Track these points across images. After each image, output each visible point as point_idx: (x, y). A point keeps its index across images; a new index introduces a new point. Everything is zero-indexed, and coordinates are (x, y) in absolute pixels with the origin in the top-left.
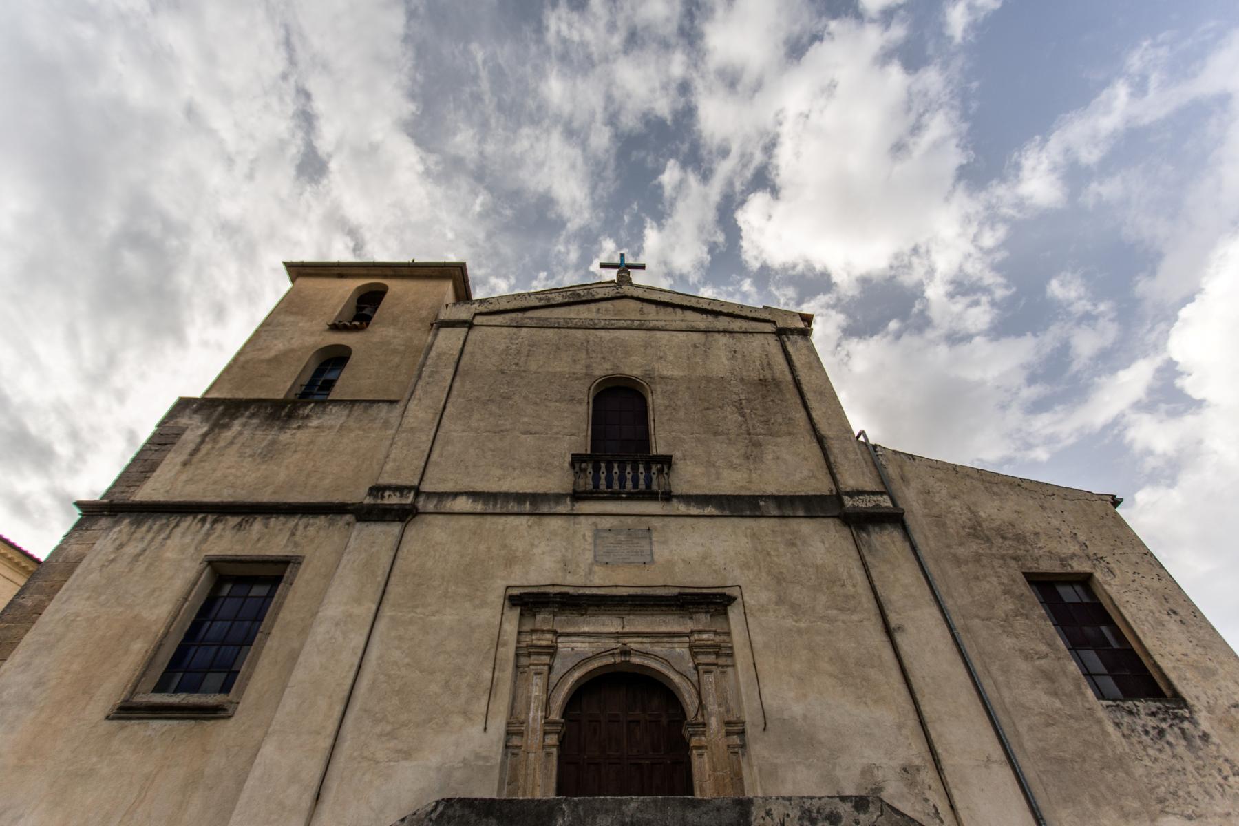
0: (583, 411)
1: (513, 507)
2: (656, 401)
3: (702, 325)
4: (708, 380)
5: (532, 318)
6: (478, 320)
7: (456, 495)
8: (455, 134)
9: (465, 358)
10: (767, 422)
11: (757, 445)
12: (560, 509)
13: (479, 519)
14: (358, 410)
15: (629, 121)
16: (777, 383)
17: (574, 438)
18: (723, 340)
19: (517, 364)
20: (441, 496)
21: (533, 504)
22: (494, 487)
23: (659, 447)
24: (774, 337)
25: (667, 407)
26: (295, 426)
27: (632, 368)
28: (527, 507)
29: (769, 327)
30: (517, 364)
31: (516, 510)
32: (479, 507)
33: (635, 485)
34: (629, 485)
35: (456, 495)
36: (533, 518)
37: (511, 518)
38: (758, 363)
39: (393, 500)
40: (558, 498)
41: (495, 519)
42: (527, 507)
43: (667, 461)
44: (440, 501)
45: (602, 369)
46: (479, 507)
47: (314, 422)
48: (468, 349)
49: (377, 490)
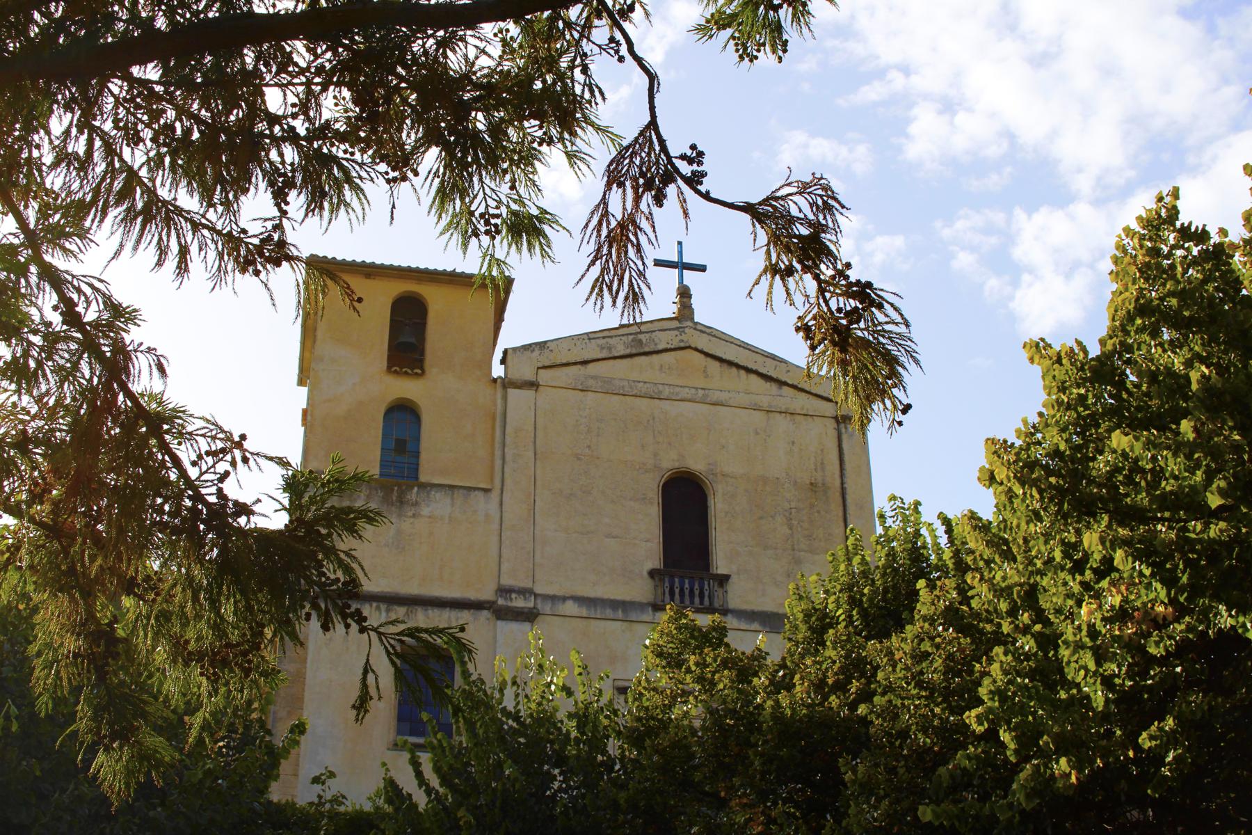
0: (654, 513)
1: (609, 613)
2: (718, 506)
3: (764, 401)
4: (765, 480)
5: (595, 377)
6: (544, 376)
7: (564, 599)
8: (965, 768)
9: (540, 434)
10: (809, 537)
11: (798, 562)
12: (645, 617)
13: (585, 622)
14: (459, 495)
15: (1026, 277)
16: (826, 488)
17: (649, 544)
18: (782, 423)
19: (589, 447)
20: (553, 599)
21: (622, 608)
22: (592, 594)
23: (721, 565)
24: (832, 423)
25: (727, 513)
26: (410, 514)
27: (697, 465)
28: (620, 614)
29: (828, 409)
30: (589, 447)
31: (612, 616)
32: (584, 612)
33: (702, 602)
34: (697, 600)
35: (564, 599)
36: (625, 624)
37: (609, 622)
38: (813, 459)
39: (519, 603)
40: (640, 606)
41: (598, 622)
42: (620, 614)
43: (723, 580)
44: (553, 604)
45: (670, 462)
46: (584, 612)
47: (425, 511)
48: (540, 422)
49: (504, 591)
